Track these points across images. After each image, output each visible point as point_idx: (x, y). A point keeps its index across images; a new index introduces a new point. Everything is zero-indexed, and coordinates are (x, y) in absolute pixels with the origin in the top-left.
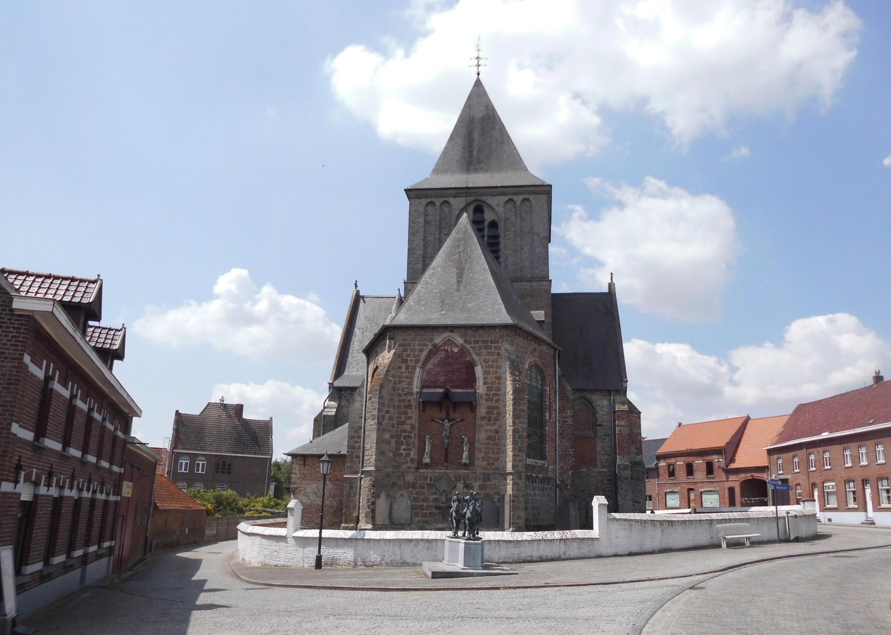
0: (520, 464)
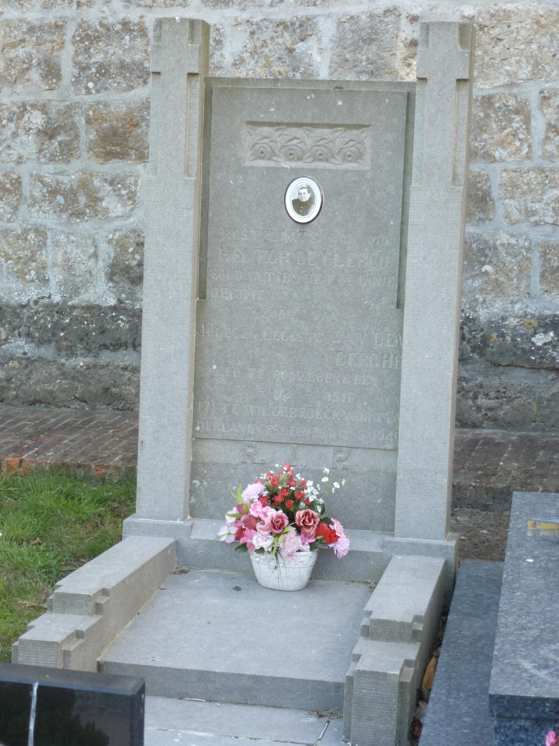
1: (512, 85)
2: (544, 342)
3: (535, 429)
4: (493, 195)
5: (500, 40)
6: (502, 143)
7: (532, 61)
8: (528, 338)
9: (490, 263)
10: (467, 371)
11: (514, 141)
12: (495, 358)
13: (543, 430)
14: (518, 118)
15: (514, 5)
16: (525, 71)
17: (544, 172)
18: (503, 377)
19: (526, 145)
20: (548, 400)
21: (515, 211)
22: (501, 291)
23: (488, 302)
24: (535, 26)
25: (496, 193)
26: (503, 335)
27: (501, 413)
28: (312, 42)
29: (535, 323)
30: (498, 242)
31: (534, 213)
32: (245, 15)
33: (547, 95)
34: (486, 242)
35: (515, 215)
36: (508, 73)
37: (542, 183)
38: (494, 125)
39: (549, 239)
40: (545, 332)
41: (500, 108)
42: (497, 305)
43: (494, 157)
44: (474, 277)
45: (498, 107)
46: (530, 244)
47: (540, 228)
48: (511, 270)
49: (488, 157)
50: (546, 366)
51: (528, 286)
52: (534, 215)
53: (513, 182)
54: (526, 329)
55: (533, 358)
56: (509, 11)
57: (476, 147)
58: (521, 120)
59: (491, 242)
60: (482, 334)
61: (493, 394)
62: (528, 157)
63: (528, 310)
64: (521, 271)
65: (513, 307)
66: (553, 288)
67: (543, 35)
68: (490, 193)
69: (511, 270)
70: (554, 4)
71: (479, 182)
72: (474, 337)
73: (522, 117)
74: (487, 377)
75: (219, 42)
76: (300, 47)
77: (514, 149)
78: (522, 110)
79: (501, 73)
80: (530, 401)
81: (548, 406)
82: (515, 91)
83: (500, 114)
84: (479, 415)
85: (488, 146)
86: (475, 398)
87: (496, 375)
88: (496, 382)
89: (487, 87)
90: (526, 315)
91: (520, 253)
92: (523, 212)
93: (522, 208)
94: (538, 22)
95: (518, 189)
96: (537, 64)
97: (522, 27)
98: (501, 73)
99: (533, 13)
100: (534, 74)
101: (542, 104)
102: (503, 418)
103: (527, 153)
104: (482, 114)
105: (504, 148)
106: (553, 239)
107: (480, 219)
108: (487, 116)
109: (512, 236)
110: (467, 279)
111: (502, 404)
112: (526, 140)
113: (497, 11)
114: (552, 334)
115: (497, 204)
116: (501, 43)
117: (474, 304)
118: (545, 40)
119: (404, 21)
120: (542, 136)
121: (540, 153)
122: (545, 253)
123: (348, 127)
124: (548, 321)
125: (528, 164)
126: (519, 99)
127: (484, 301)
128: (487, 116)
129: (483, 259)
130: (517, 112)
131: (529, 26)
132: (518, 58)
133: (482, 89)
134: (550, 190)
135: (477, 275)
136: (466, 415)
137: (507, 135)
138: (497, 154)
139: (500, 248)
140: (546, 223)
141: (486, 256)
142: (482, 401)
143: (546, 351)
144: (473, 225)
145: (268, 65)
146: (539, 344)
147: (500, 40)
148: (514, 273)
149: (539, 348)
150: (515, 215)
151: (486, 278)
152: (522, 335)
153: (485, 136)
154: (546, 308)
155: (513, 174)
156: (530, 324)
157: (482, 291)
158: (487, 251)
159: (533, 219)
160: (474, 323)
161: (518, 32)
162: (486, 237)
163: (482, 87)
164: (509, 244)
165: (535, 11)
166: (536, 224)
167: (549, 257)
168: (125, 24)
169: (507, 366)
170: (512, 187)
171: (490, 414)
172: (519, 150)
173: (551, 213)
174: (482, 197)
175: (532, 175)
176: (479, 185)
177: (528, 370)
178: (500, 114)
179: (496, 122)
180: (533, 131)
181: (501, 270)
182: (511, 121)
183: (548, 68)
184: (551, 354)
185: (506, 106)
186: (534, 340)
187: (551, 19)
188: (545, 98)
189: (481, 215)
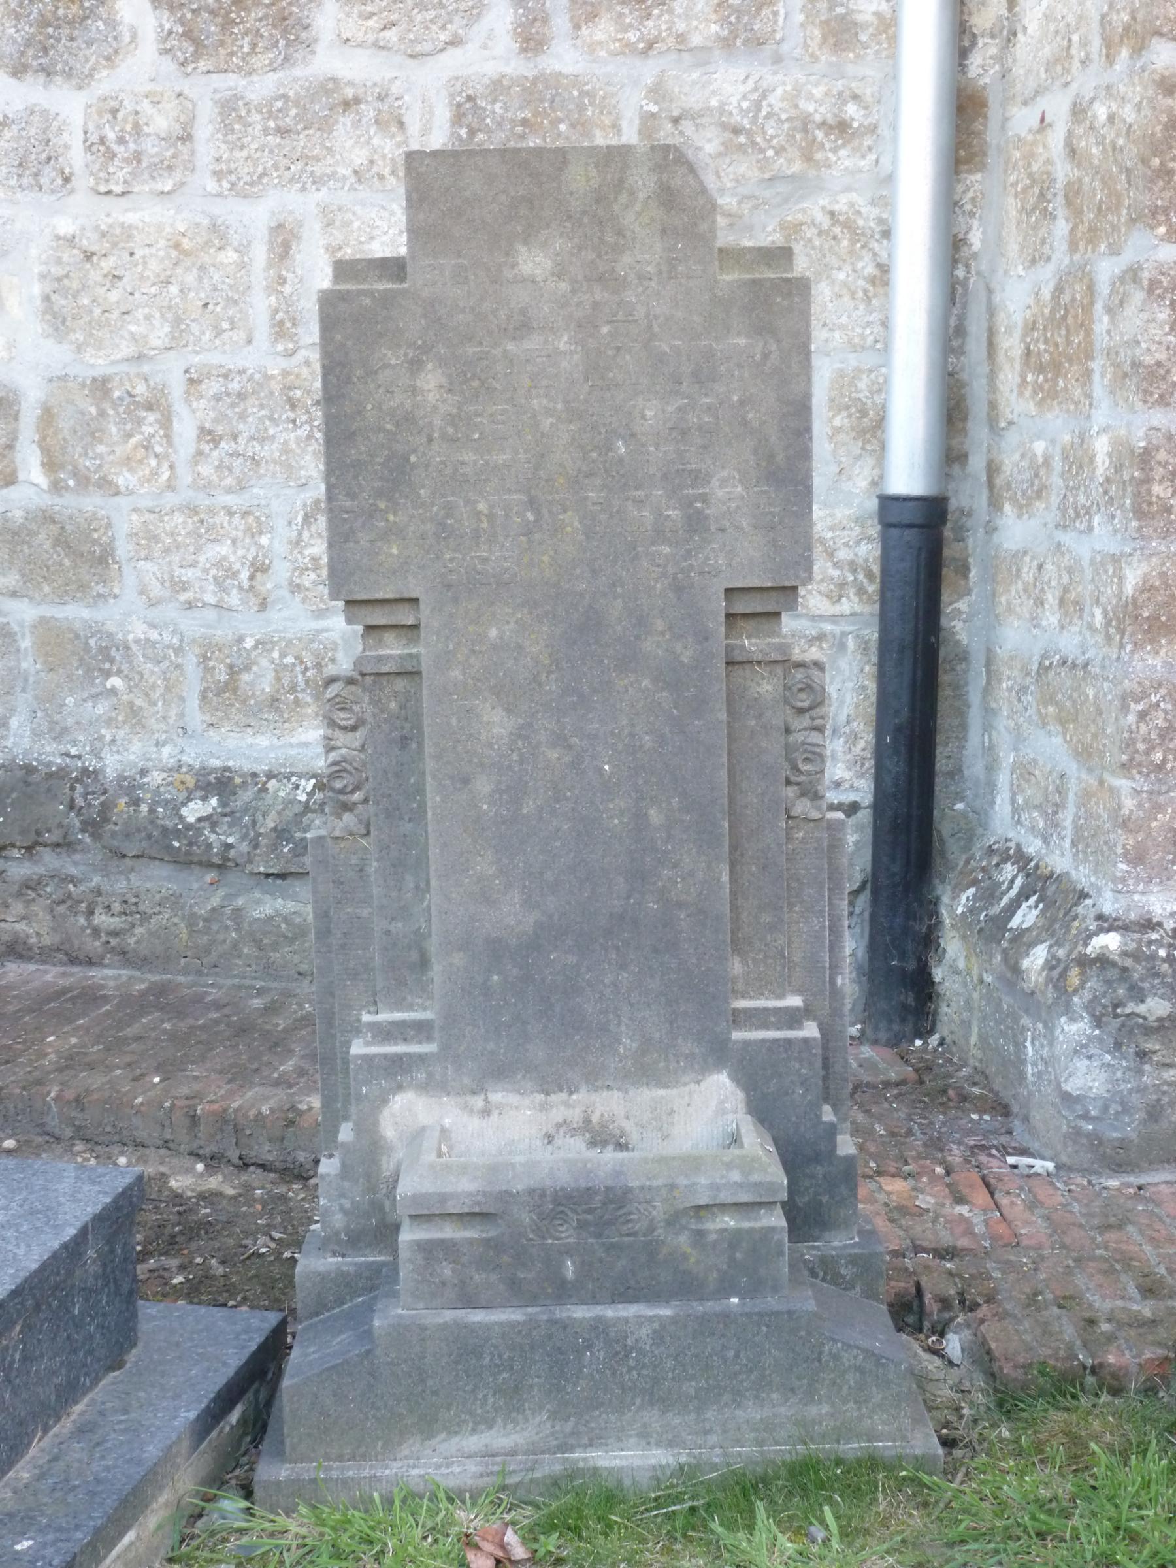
1: (140, 358)
2: (198, 815)
3: (185, 972)
4: (118, 552)
5: (119, 278)
6: (127, 462)
7: (169, 316)
8: (175, 809)
9: (119, 672)
10: (76, 864)
11: (147, 457)
12: (115, 843)
13: (199, 973)
14: (151, 417)
15: (138, 215)
16: (159, 334)
17: (197, 513)
18: (132, 876)
19: (166, 465)
20: (205, 920)
21: (155, 582)
22: (139, 722)
23: (119, 743)
24: (174, 254)
25: (123, 549)
26: (136, 802)
27: (132, 941)
29: (191, 781)
30: (131, 637)
31: (184, 586)
33: (195, 376)
34: (110, 635)
35: (156, 590)
36: (134, 338)
37: (194, 533)
38: (114, 430)
39: (212, 631)
40: (204, 799)
41: (121, 399)
42: (134, 748)
43: (117, 486)
44: (95, 697)
45: (119, 398)
46: (181, 641)
47: (196, 613)
48: (153, 687)
49: (107, 486)
50: (196, 859)
51: (181, 715)
52: (184, 589)
53: (149, 531)
54: (174, 792)
55: (177, 844)
56: (130, 226)
57: (88, 469)
58: (157, 421)
59: (120, 636)
60: (102, 798)
61: (117, 907)
62: (170, 487)
63: (184, 758)
64: (168, 688)
65: (159, 752)
66: (221, 719)
67: (188, 269)
68: (113, 550)
69: (153, 687)
70: (203, 212)
71: (95, 530)
72: (90, 805)
73: (158, 415)
74: (107, 875)
77: (147, 472)
78: (156, 403)
79: (122, 337)
80: (176, 920)
81: (207, 930)
82: (146, 368)
83: (121, 410)
84: (97, 944)
85: (106, 466)
86: (90, 913)
87: (121, 873)
88: (121, 885)
89: (100, 361)
90: (180, 767)
91: (164, 657)
92: (167, 584)
93: (166, 577)
94: (177, 246)
95: (157, 542)
96: (178, 321)
97: (151, 255)
98: (122, 337)
99: (168, 229)
100: (173, 338)
101: (187, 392)
102: (134, 950)
103: (169, 479)
104: (93, 410)
105: (131, 470)
106: (219, 633)
107: (99, 595)
108: (102, 413)
109: (153, 626)
110: (85, 700)
111: (133, 926)
112: (166, 456)
113: (111, 226)
114: (214, 801)
115: (126, 569)
116: (119, 284)
117: (98, 745)
118: (190, 278)
120: (192, 451)
121: (190, 479)
122: (205, 658)
124: (212, 778)
125: (170, 500)
126: (152, 383)
127: (113, 741)
128: (102, 413)
129: (107, 666)
130: (149, 407)
131: (162, 253)
132: (147, 310)
133: (92, 365)
134: (210, 545)
135: (101, 694)
136: (76, 943)
137: (136, 447)
138: (121, 481)
139: (134, 647)
140: (205, 604)
141: (112, 661)
142: (101, 919)
143: (199, 832)
144: (89, 606)
146: (191, 819)
147: (119, 278)
148: (159, 692)
149: (189, 827)
150: (156, 590)
151: (115, 700)
152: (167, 802)
153: (101, 449)
154: (212, 755)
155: (148, 516)
156: (182, 782)
157: (109, 722)
158: (113, 652)
159: (183, 597)
160: (96, 779)
161: (145, 263)
162: (111, 626)
163: (92, 361)
164: (147, 640)
165: (172, 225)
166: (190, 605)
167: (211, 664)
169: (137, 856)
170: (147, 538)
171: (114, 942)
172: (155, 473)
173: (212, 587)
174: (101, 557)
175: (179, 519)
176: (96, 536)
177: (172, 866)
178: (121, 410)
179: (116, 424)
180: (176, 440)
181: (136, 686)
182: (139, 422)
183: (195, 328)
184: (207, 838)
185: (131, 396)
186: (184, 811)
187: (199, 240)
188: (191, 381)
189: (100, 588)
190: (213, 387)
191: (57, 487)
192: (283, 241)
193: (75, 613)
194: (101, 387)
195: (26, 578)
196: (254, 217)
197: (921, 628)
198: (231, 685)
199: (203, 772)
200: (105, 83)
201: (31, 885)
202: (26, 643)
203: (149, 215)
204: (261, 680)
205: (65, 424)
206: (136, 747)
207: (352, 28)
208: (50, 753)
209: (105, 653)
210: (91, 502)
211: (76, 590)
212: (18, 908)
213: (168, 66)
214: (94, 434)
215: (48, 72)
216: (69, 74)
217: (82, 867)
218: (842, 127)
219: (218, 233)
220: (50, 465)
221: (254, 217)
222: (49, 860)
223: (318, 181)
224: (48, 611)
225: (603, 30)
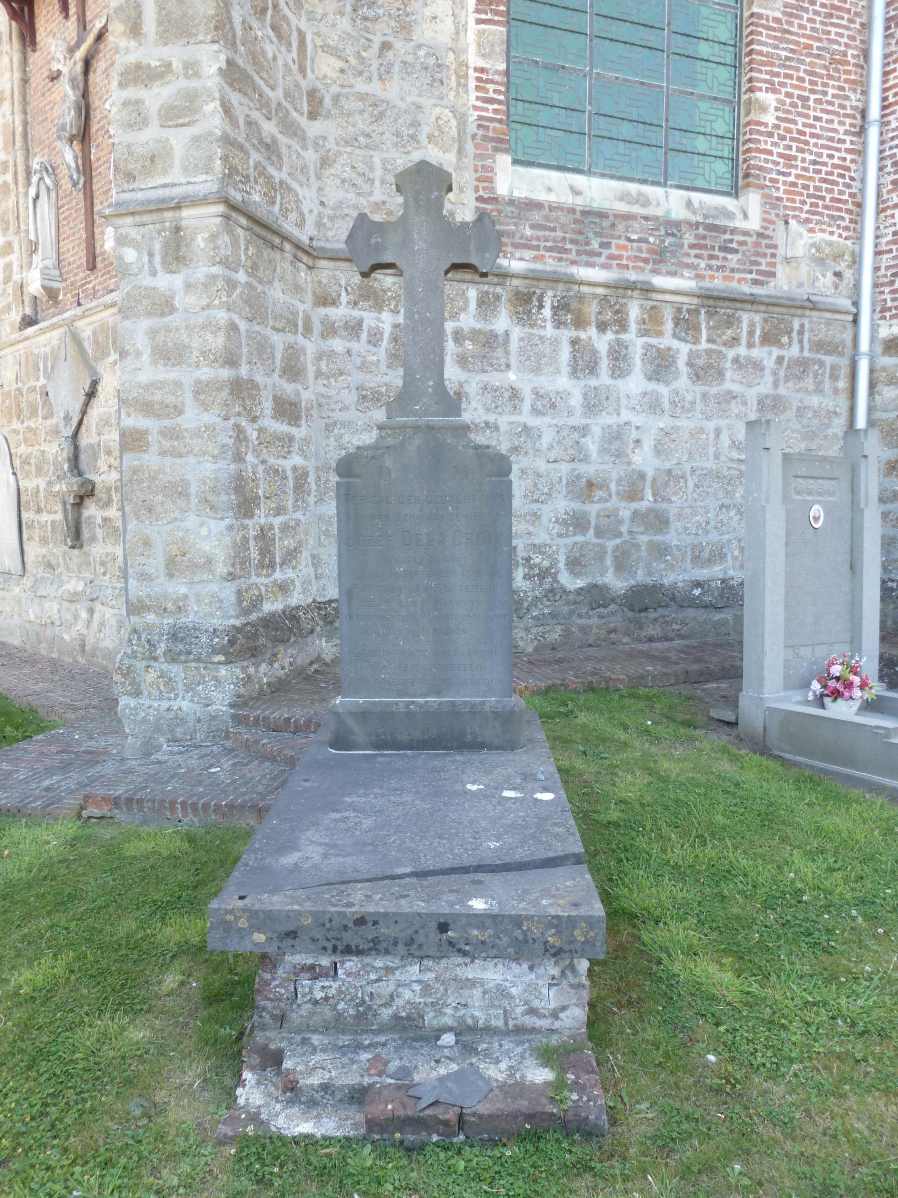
0: (178, 140)
1: (679, 464)
6: (675, 493)
28: (588, 438)
32: (554, 422)
49: (669, 501)
62: (686, 500)
75: (540, 436)
76: (583, 440)
88: (680, 616)
119: (633, 429)
123: (830, 479)
125: (686, 504)
142: (675, 626)
145: (566, 450)
150: (680, 530)
157: (665, 569)
168: (487, 423)
190: (698, 472)
191: (655, 501)
192: (718, 432)
193: (659, 538)
194: (669, 471)
195: (647, 529)
196: (711, 425)
197: (80, 162)
198: (698, 557)
199: (692, 582)
200: (675, 385)
201: (656, 620)
202: (643, 548)
203: (686, 424)
204: (706, 555)
205: (659, 483)
206: (672, 576)
207: (736, 377)
208: (649, 581)
209: (666, 549)
210: (664, 506)
211: (660, 531)
212: (651, 627)
213: (689, 382)
214: (666, 485)
215: (658, 380)
216: (664, 382)
217: (670, 613)
218: (835, 413)
219: (701, 430)
220: (654, 495)
221: (711, 425)
222: (661, 611)
223: (727, 417)
224: (651, 538)
225: (790, 385)
